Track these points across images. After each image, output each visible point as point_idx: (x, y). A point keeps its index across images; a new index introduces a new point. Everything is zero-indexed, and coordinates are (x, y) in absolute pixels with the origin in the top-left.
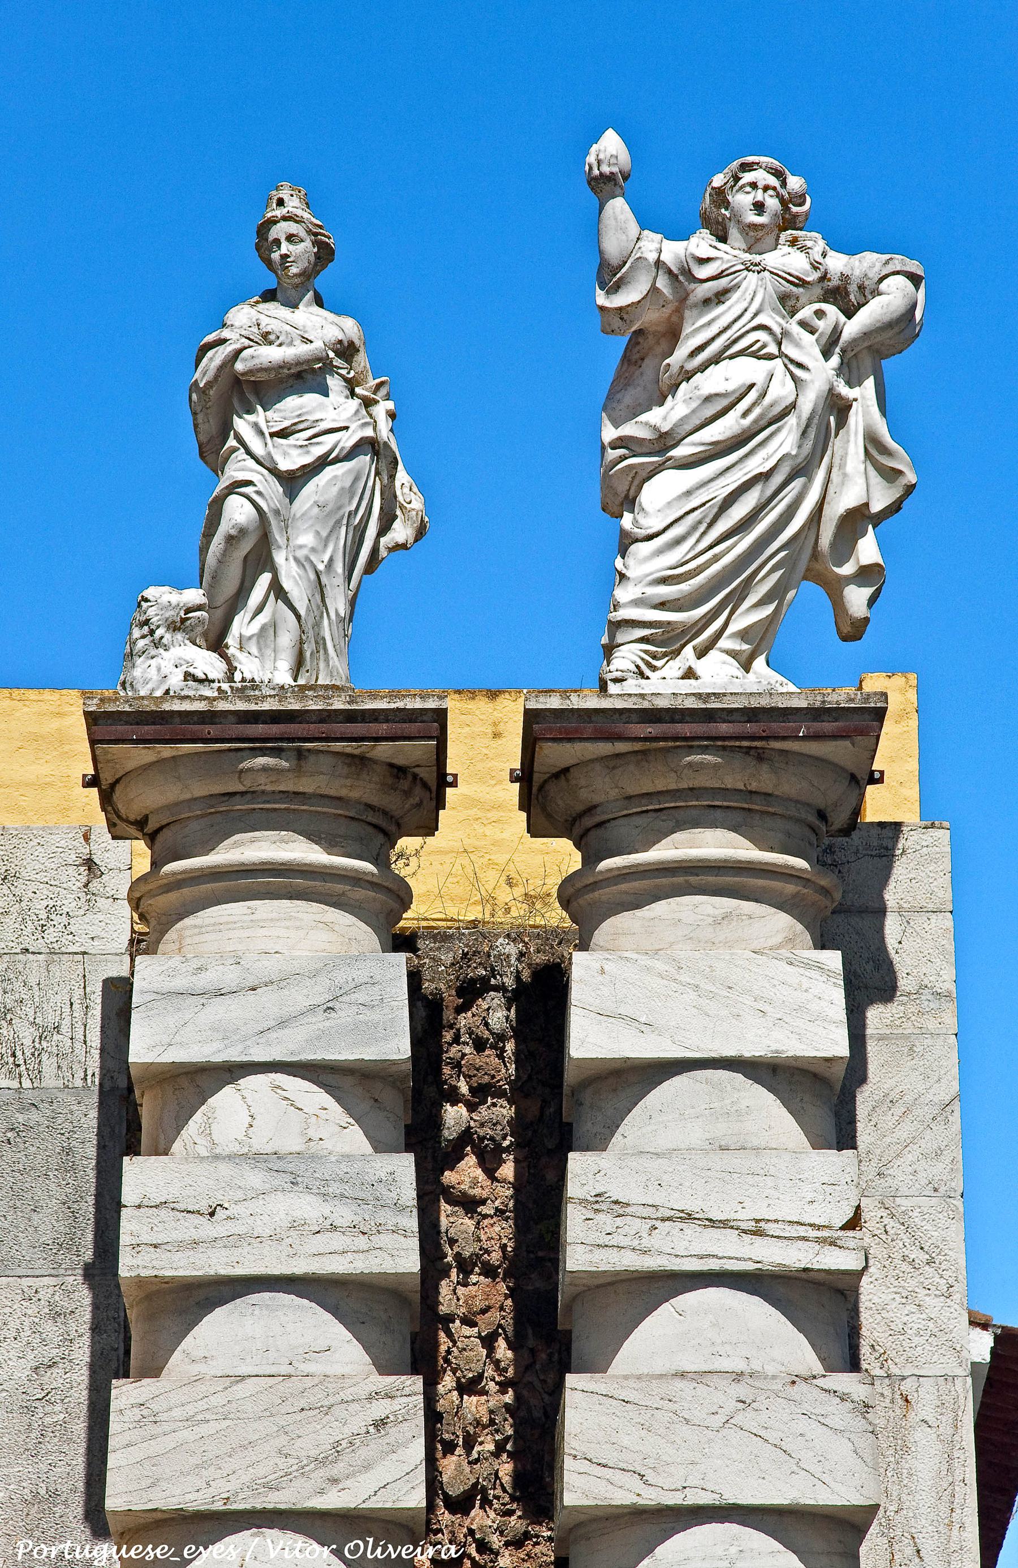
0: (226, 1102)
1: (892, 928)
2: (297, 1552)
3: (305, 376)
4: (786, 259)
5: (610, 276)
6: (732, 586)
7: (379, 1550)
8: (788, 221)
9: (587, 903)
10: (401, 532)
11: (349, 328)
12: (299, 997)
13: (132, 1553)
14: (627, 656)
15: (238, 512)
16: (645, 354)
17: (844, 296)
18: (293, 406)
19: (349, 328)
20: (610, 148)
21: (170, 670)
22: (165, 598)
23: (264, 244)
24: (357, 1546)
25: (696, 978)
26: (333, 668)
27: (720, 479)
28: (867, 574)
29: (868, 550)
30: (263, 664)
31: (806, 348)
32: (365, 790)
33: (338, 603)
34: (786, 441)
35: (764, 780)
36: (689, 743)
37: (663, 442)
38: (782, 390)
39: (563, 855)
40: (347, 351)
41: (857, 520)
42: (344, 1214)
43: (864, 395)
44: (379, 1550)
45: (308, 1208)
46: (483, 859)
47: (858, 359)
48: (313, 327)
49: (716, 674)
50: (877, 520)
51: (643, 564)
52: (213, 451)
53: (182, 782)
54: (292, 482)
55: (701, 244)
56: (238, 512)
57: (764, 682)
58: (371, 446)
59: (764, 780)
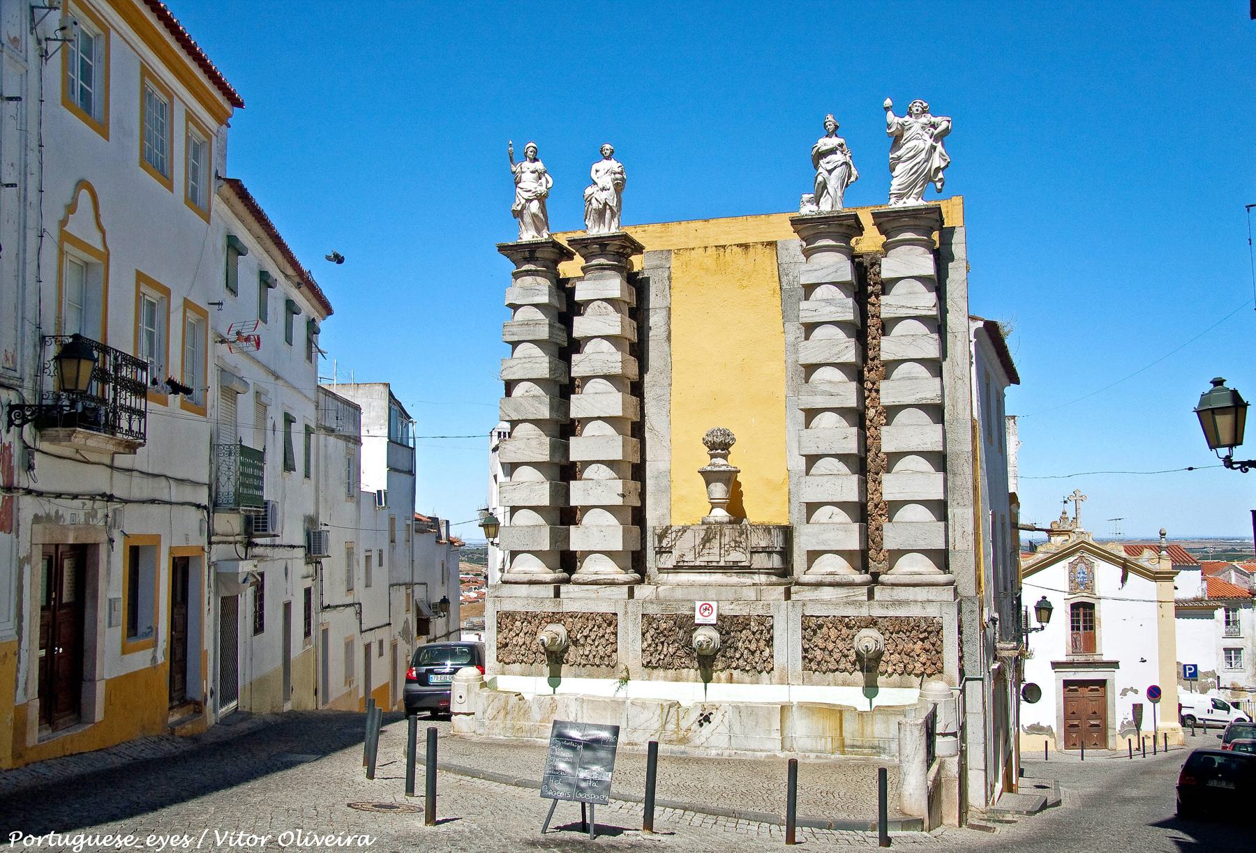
0: (818, 289)
1: (953, 247)
2: (239, 840)
3: (832, 151)
4: (923, 120)
5: (889, 126)
6: (912, 185)
7: (307, 840)
8: (924, 112)
9: (887, 248)
10: (853, 179)
11: (842, 141)
12: (830, 270)
13: (104, 841)
14: (893, 200)
15: (820, 179)
16: (897, 140)
17: (934, 126)
18: (830, 158)
19: (842, 141)
20: (888, 102)
21: (807, 210)
22: (806, 197)
23: (825, 127)
24: (289, 837)
25: (908, 262)
26: (839, 207)
27: (909, 165)
28: (940, 180)
29: (940, 175)
30: (826, 206)
31: (927, 137)
32: (842, 230)
33: (839, 194)
34: (923, 156)
35: (917, 222)
36: (902, 217)
37: (899, 158)
38: (922, 146)
39: (884, 238)
40: (841, 145)
41: (938, 170)
42: (840, 310)
43: (939, 145)
44: (307, 840)
45: (833, 309)
46: (870, 240)
47: (937, 138)
48: (834, 142)
49: (912, 202)
50: (943, 169)
51: (895, 182)
52: (816, 167)
53: (809, 229)
54: (830, 172)
55: (907, 118)
56: (820, 179)
57: (921, 203)
58: (845, 163)
59: (917, 222)
